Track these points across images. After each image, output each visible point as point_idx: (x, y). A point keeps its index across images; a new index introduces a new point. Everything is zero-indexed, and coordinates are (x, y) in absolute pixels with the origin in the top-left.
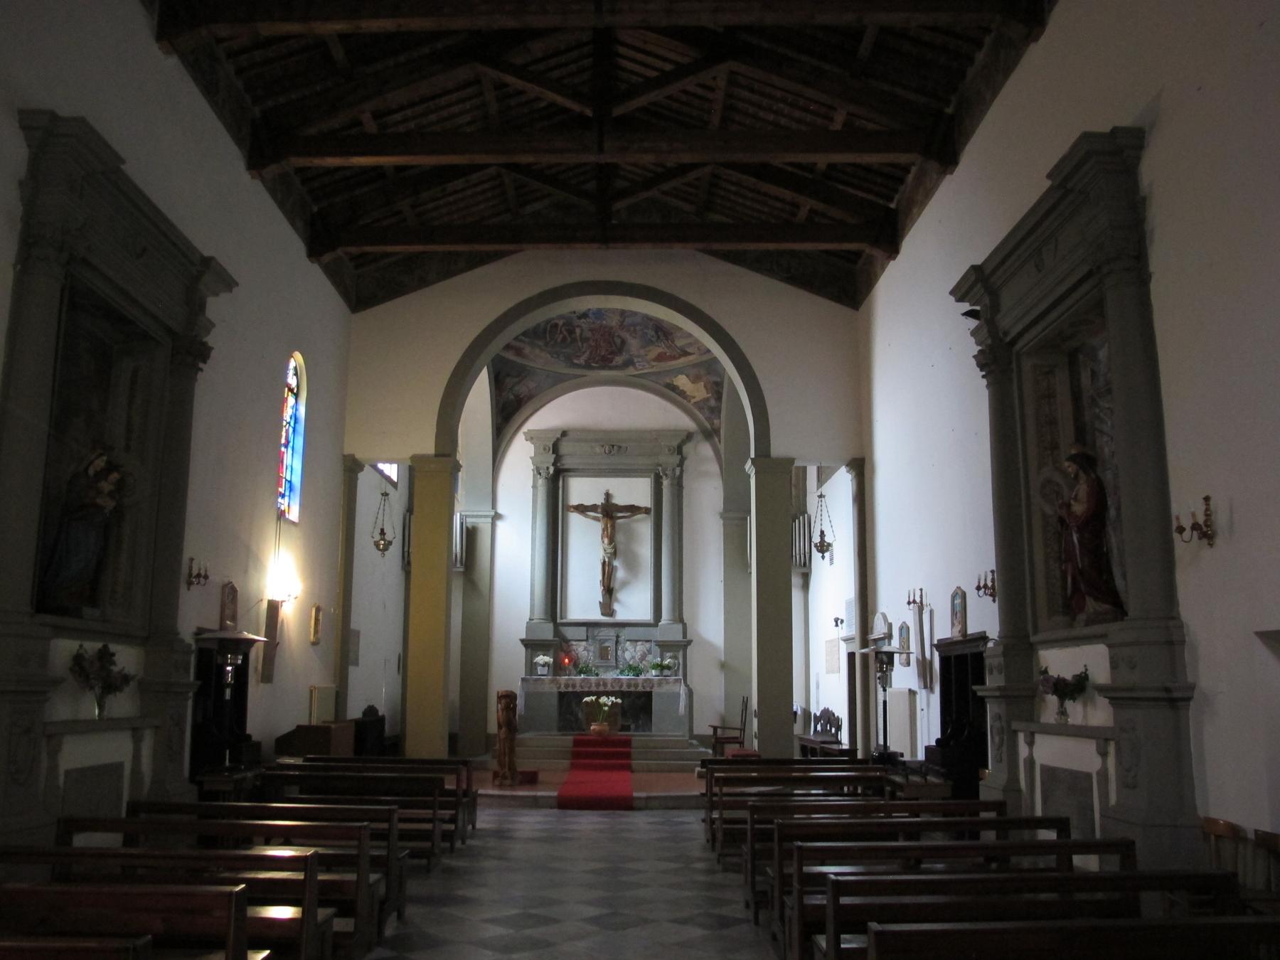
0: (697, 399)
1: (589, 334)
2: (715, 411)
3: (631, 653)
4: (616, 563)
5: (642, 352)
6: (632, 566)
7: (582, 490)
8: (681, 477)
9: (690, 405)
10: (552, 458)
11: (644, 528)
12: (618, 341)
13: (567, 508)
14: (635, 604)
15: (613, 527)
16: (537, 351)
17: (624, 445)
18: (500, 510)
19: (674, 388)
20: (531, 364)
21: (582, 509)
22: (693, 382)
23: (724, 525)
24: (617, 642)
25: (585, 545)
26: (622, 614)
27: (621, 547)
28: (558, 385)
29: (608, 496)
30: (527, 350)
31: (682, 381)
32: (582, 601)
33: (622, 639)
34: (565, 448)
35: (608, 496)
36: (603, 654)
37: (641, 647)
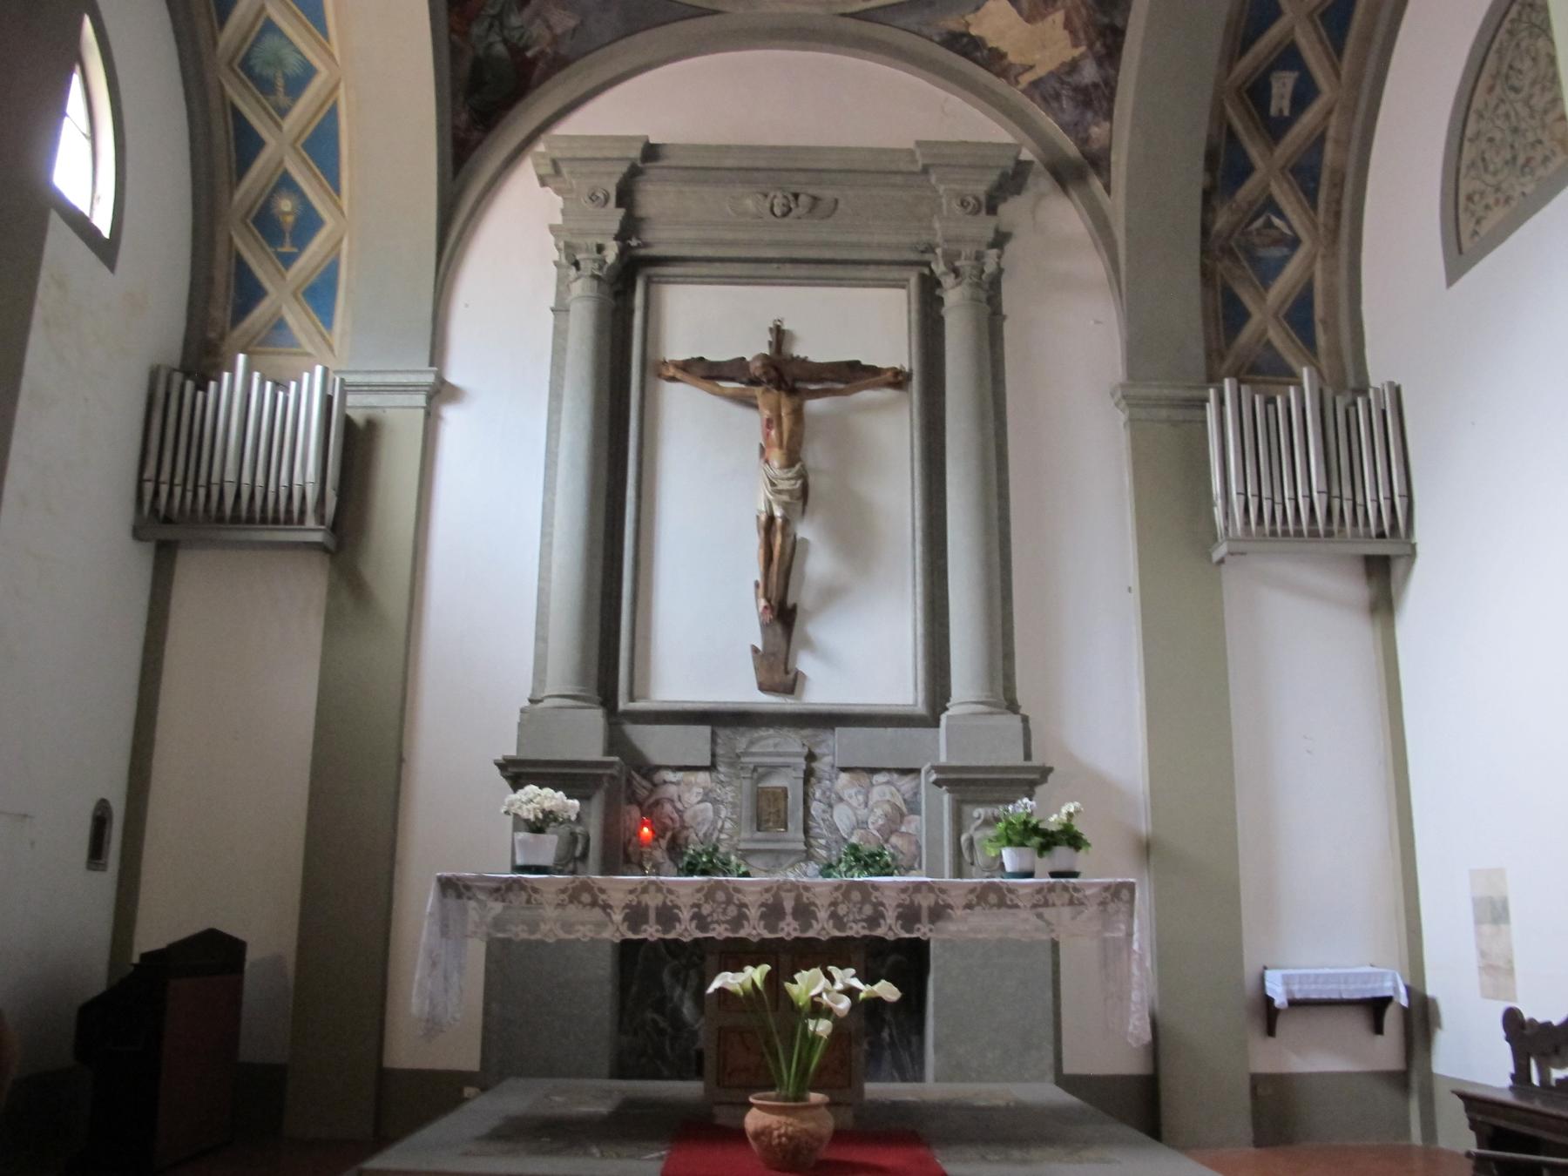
0: (1040, 72)
2: (1097, 99)
3: (852, 810)
4: (805, 531)
6: (855, 540)
7: (700, 318)
8: (995, 283)
9: (1016, 95)
10: (614, 217)
11: (891, 429)
13: (656, 370)
14: (865, 655)
15: (798, 414)
17: (828, 194)
18: (454, 377)
19: (966, 45)
21: (705, 372)
22: (1028, 20)
23: (1132, 421)
24: (809, 774)
25: (709, 480)
26: (823, 688)
27: (818, 484)
29: (779, 335)
32: (699, 644)
33: (822, 766)
34: (654, 199)
35: (779, 335)
36: (767, 811)
37: (884, 791)
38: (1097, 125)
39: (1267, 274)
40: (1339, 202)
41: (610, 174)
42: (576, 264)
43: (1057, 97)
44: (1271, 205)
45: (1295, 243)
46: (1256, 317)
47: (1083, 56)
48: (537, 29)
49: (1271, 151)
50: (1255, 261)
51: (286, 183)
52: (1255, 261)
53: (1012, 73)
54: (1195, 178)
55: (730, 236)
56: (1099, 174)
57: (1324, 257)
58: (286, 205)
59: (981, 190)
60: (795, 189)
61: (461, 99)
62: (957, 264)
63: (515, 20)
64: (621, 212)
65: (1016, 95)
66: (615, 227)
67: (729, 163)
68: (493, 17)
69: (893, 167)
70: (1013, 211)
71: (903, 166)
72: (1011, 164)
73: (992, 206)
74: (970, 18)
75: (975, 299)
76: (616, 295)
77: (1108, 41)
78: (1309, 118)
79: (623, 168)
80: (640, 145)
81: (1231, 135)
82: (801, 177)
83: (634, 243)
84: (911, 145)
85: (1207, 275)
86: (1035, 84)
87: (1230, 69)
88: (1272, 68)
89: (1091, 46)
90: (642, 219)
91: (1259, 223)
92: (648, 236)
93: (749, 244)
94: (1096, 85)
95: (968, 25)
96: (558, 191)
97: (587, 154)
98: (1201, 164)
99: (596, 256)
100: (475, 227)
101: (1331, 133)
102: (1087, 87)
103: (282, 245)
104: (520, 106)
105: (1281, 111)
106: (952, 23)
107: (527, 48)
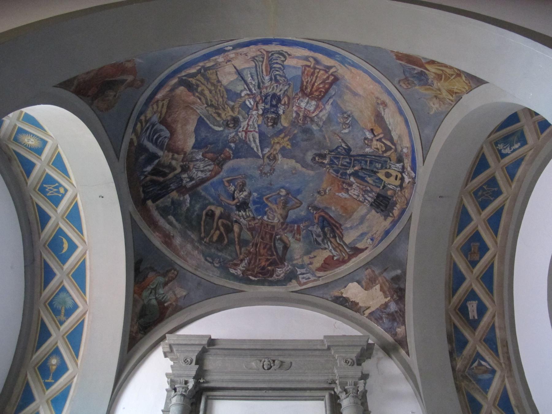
0: (372, 309)
1: (247, 235)
2: (398, 317)
5: (306, 259)
8: (365, 393)
9: (364, 319)
10: (193, 369)
12: (280, 246)
16: (189, 247)
17: (287, 360)
19: (343, 301)
20: (179, 262)
22: (365, 290)
28: (213, 297)
30: (178, 241)
31: (353, 291)
34: (213, 363)
38: (399, 328)
39: (486, 386)
40: (508, 353)
41: (194, 351)
42: (175, 390)
43: (381, 318)
44: (479, 356)
45: (493, 372)
46: (485, 407)
47: (389, 301)
48: (170, 295)
49: (474, 334)
50: (478, 381)
51: (56, 352)
52: (478, 381)
53: (362, 310)
54: (445, 347)
55: (245, 378)
56: (403, 347)
57: (508, 377)
58: (54, 361)
59: (354, 356)
60: (274, 359)
61: (135, 320)
62: (346, 387)
63: (161, 291)
64: (197, 366)
65: (364, 319)
66: (194, 373)
67: (245, 347)
68: (152, 289)
69: (315, 348)
70: (368, 365)
71: (319, 347)
72: (365, 344)
73: (359, 361)
74: (343, 290)
75: (356, 403)
76: (192, 404)
77: (399, 294)
78: (486, 319)
79: (199, 349)
80: (208, 339)
81: (455, 327)
82: (277, 353)
83: (202, 381)
84: (322, 338)
85: (459, 389)
86: (371, 314)
87: (450, 302)
88: (466, 300)
89: (392, 297)
90: (206, 370)
91: (476, 364)
92: (208, 378)
93: (253, 381)
94: (396, 312)
95: (342, 293)
96: (172, 359)
97: (184, 343)
98: (446, 342)
99: (184, 386)
100: (133, 376)
101: (497, 325)
102: (393, 312)
103: (48, 379)
104: (160, 325)
105: (474, 317)
106: (336, 293)
107: (165, 302)
